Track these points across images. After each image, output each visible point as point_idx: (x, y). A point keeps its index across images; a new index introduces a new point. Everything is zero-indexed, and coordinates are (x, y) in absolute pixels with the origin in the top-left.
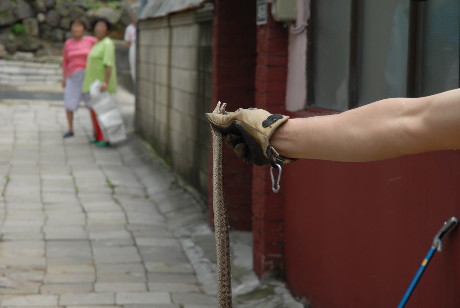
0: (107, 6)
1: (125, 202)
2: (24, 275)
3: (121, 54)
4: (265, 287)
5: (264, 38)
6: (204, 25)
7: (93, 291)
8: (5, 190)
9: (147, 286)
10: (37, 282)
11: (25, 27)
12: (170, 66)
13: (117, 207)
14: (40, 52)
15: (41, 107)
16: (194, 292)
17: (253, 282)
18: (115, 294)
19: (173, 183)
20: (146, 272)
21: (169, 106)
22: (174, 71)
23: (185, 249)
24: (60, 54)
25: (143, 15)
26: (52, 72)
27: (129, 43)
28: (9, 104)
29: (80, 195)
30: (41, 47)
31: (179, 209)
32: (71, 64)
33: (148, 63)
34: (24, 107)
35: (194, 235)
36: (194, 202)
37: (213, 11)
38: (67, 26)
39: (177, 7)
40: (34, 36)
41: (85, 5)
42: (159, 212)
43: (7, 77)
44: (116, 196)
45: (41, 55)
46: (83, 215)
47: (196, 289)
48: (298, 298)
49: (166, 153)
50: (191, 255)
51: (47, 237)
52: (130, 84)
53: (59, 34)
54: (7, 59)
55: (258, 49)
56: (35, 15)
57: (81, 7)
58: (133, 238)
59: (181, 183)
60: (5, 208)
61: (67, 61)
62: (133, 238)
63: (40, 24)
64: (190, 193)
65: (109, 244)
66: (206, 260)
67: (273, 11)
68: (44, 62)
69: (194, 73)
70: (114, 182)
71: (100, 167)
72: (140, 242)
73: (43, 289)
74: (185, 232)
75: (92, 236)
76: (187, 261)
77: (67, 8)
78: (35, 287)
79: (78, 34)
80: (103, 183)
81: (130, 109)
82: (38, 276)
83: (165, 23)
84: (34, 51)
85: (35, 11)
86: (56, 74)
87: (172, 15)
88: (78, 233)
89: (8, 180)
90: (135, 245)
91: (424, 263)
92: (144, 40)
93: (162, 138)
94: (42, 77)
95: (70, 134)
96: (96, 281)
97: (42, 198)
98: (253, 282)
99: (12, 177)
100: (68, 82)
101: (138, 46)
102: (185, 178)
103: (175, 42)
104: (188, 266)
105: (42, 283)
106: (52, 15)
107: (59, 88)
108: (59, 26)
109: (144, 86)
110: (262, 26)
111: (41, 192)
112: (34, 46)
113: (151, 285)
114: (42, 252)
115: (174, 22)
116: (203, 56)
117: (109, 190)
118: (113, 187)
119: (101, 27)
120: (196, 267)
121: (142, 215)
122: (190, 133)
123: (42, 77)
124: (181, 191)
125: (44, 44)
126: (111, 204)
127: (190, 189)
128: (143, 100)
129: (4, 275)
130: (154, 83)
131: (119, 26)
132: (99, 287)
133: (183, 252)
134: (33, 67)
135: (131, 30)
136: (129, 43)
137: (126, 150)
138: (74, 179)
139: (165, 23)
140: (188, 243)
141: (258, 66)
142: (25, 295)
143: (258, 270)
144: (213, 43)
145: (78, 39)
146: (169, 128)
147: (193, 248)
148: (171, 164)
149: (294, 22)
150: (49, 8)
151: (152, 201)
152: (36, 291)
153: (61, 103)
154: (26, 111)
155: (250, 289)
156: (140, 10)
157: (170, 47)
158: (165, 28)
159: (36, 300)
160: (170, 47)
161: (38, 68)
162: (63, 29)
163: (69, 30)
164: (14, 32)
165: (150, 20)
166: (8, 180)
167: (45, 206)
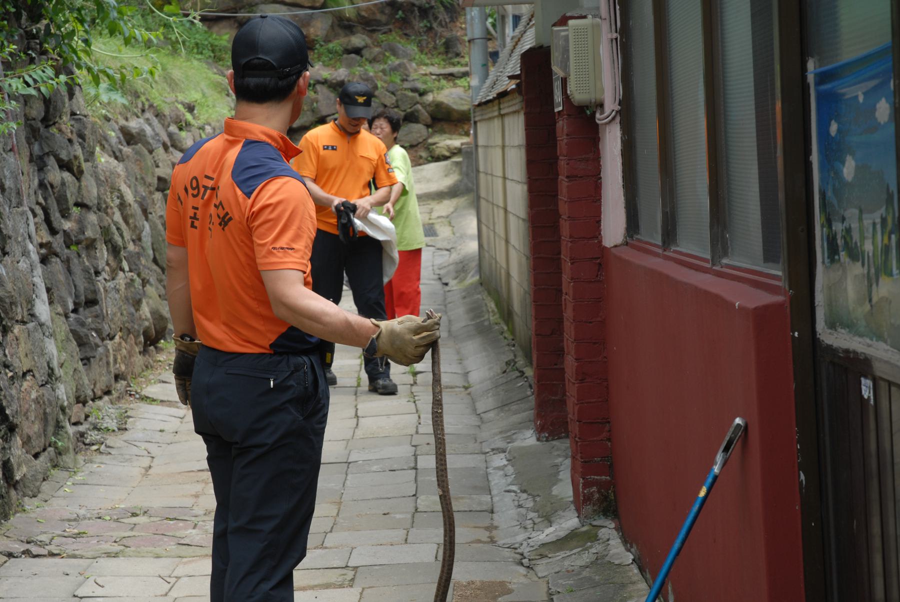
0: (455, 85)
4: (585, 529)
17: (569, 522)
21: (507, 241)
23: (490, 470)
41: (421, 86)
42: (475, 410)
47: (484, 535)
50: (498, 481)
57: (414, 90)
69: (525, 187)
74: (500, 444)
77: (393, 93)
90: (415, 468)
91: (702, 494)
96: (331, 531)
98: (569, 522)
110: (559, 112)
129: (195, 527)
140: (499, 460)
143: (581, 502)
146: (508, 275)
149: (601, 105)
155: (562, 534)
157: (503, 147)
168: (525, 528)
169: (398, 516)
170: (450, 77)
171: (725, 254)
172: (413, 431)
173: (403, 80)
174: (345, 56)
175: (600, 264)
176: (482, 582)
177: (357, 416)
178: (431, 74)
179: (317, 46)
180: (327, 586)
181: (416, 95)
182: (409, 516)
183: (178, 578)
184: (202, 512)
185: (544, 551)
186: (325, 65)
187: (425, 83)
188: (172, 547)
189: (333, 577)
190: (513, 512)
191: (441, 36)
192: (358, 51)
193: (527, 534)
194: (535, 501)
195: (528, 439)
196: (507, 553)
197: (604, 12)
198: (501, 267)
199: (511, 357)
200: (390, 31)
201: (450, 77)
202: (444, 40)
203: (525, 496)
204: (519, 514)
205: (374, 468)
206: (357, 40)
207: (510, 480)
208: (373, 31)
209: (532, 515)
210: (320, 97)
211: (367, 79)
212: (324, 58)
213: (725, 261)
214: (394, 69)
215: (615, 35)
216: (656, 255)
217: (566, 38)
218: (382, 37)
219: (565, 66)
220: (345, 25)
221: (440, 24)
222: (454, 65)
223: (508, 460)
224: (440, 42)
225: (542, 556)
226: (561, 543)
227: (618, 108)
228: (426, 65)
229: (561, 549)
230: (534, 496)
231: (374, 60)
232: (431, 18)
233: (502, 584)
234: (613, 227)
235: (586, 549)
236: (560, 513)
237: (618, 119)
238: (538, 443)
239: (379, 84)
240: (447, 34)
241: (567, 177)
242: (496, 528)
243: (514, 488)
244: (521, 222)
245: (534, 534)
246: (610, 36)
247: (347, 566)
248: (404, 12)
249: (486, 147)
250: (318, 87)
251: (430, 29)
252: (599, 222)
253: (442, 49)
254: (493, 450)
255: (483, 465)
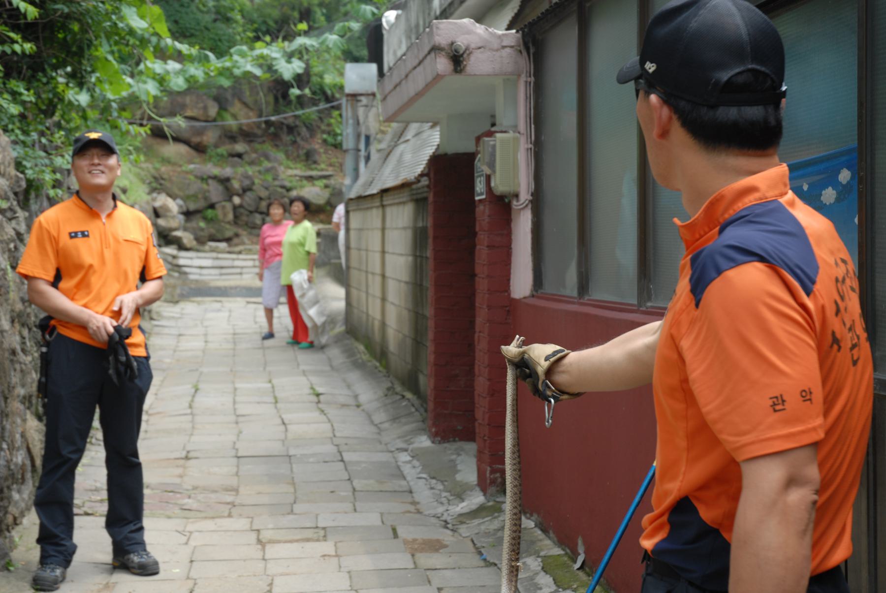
0: (314, 185)
1: (332, 412)
2: (213, 496)
3: (327, 239)
4: (491, 504)
5: (483, 214)
6: (420, 202)
7: (292, 512)
8: (192, 401)
9: (354, 506)
10: (228, 503)
11: (219, 212)
12: (383, 252)
13: (323, 418)
14: (236, 241)
15: (237, 304)
16: (410, 512)
17: (477, 499)
18: (317, 516)
19: (388, 389)
20: (354, 490)
21: (384, 299)
22: (387, 256)
23: (400, 464)
24: (256, 244)
25: (353, 195)
26: (251, 263)
27: (338, 225)
28: (199, 303)
29: (279, 405)
30: (237, 235)
31: (394, 419)
32: (269, 253)
33: (359, 250)
34: (217, 305)
35: (411, 447)
36: (413, 410)
37: (428, 186)
38: (264, 210)
39: (390, 184)
40: (229, 223)
41: (288, 184)
42: (372, 422)
43: (198, 271)
44: (320, 406)
45: (237, 245)
46: (282, 428)
47: (412, 508)
48: (528, 515)
49: (381, 354)
50: (407, 470)
51: (239, 454)
52: (341, 276)
53: (258, 219)
54: (198, 251)
55: (477, 229)
56: (230, 199)
57: (283, 187)
58: (340, 453)
59: (398, 388)
60: (192, 421)
61: (264, 250)
62: (340, 453)
63: (235, 208)
64: (408, 399)
65: (311, 460)
66: (424, 476)
67: (493, 184)
68: (240, 253)
69: (410, 259)
70: (320, 390)
71: (304, 373)
72: (347, 457)
73: (234, 511)
74: (404, 446)
75: (292, 452)
76: (404, 478)
77: (267, 188)
78: (225, 509)
79: (277, 218)
80: (308, 391)
81: (341, 305)
82: (229, 499)
83: (377, 203)
84: (228, 240)
85: (229, 193)
86: (255, 267)
87: (385, 191)
88: (276, 448)
89: (197, 390)
90: (342, 460)
92: (354, 224)
93: (377, 337)
94: (238, 270)
95: (270, 335)
96: (295, 502)
97: (235, 409)
98: (477, 499)
99: (201, 386)
100: (266, 274)
101: (348, 230)
102: (403, 384)
103: (388, 224)
104: (404, 483)
105: (233, 504)
106: (249, 197)
107: (257, 283)
108: (257, 211)
109: (354, 275)
110: (480, 201)
111: (235, 402)
112: (228, 234)
113: (358, 504)
114: (235, 470)
115: (387, 200)
116: (419, 238)
117: (315, 399)
118: (318, 395)
119: (298, 207)
120: (412, 483)
121: (352, 427)
122: (407, 330)
123: (238, 270)
124: (399, 397)
125: (240, 231)
126: (316, 415)
127: (409, 395)
128: (354, 292)
129: (189, 497)
130: (367, 272)
131: (328, 208)
132: (297, 508)
133: (398, 467)
134: (227, 259)
135: (340, 209)
136: (338, 225)
137: (335, 353)
138: (273, 387)
139: (377, 203)
140: (404, 457)
141: (478, 247)
142: (213, 518)
144: (430, 223)
145: (277, 223)
146: (383, 324)
147: (409, 462)
148: (387, 367)
149: (517, 196)
150: (246, 190)
151: (363, 410)
152: (226, 514)
153: (260, 300)
154: (219, 310)
155: (474, 507)
156: (350, 187)
157: (383, 229)
158: (377, 207)
159: (227, 523)
160: (383, 229)
161: (234, 259)
162: (261, 213)
163: (268, 214)
164: (205, 219)
165: (360, 198)
166: (197, 390)
167: (238, 418)
168: (442, 503)
169: (342, 494)
170: (310, 178)
171: (649, 299)
172: (331, 435)
173: (274, 179)
174: (230, 159)
175: (508, 311)
176: (424, 540)
177: (284, 423)
178: (296, 176)
179: (209, 150)
180: (308, 540)
181: (284, 191)
182: (351, 494)
183: (191, 533)
184: (190, 488)
185: (461, 519)
186: (215, 165)
187: (291, 182)
188: (177, 511)
189: (309, 534)
190: (428, 493)
191: (303, 148)
192: (240, 156)
193: (445, 508)
194: (444, 485)
195: (424, 442)
196: (434, 520)
197: (522, 127)
198: (374, 319)
199: (390, 385)
200: (264, 142)
201: (310, 178)
202: (305, 151)
203: (434, 481)
204: (433, 494)
205: (311, 460)
206: (240, 147)
207: (419, 470)
208: (251, 141)
209: (444, 494)
210: (211, 188)
211: (247, 177)
212: (213, 159)
213: (649, 304)
214: (268, 170)
215: (530, 146)
216: (573, 303)
217: (494, 147)
218: (257, 146)
219: (492, 165)
220: (230, 137)
221: (302, 139)
222: (312, 169)
223: (413, 457)
224: (302, 152)
225: (462, 523)
226: (475, 513)
227: (530, 198)
228: (291, 168)
229: (475, 518)
230: (442, 482)
231: (252, 163)
232: (296, 133)
233: (438, 541)
234: (521, 283)
235: (495, 518)
236: (469, 492)
237: (530, 206)
238: (433, 445)
239: (256, 181)
240: (308, 147)
241: (488, 246)
242: (418, 503)
243: (424, 476)
244: (402, 284)
245: (450, 508)
246: (526, 146)
247: (317, 527)
248: (275, 128)
249: (360, 230)
250: (210, 181)
251: (295, 142)
252: (509, 280)
253: (303, 158)
254: (398, 449)
255: (393, 460)
